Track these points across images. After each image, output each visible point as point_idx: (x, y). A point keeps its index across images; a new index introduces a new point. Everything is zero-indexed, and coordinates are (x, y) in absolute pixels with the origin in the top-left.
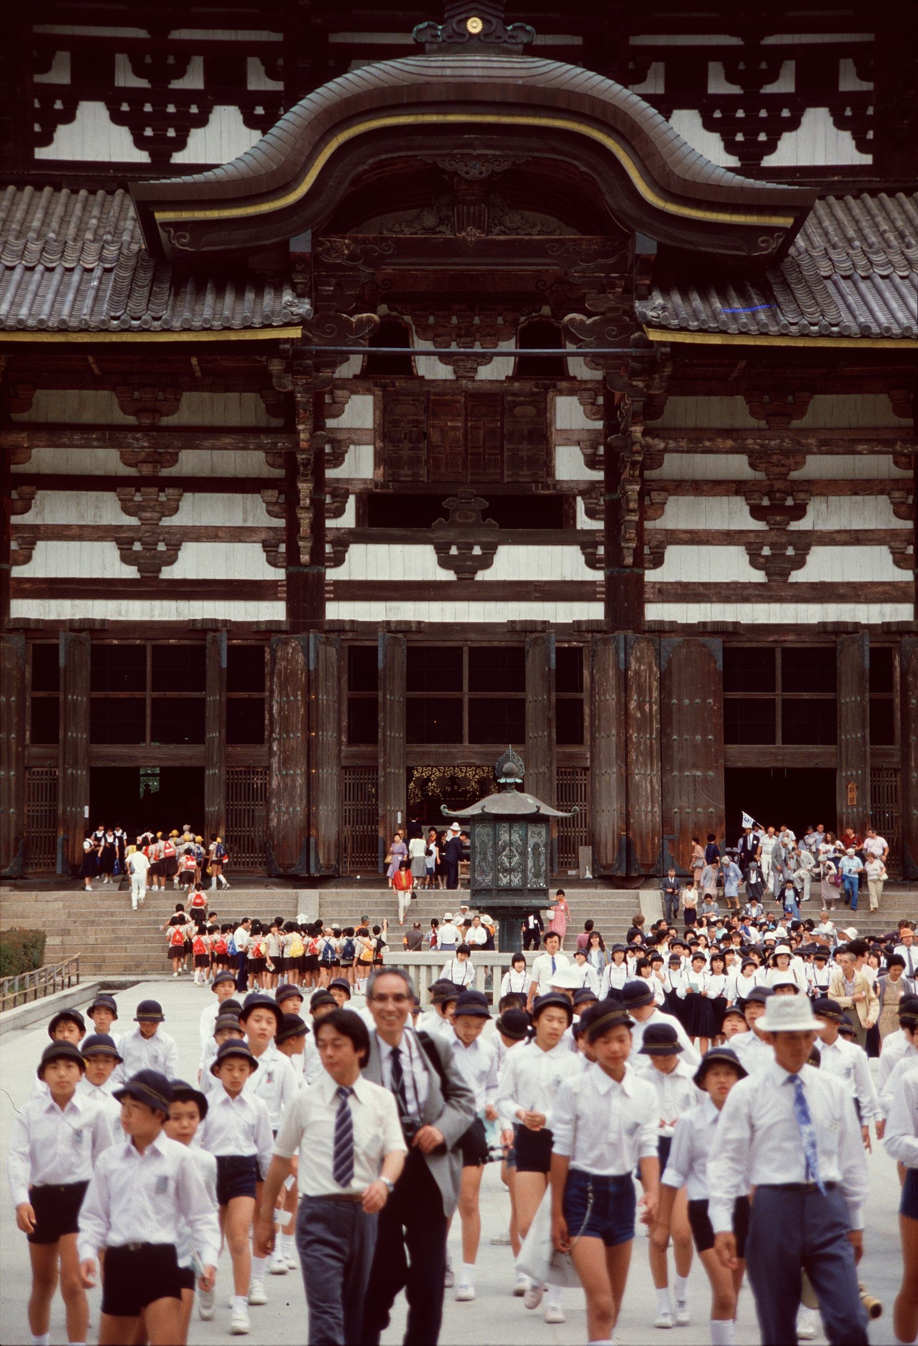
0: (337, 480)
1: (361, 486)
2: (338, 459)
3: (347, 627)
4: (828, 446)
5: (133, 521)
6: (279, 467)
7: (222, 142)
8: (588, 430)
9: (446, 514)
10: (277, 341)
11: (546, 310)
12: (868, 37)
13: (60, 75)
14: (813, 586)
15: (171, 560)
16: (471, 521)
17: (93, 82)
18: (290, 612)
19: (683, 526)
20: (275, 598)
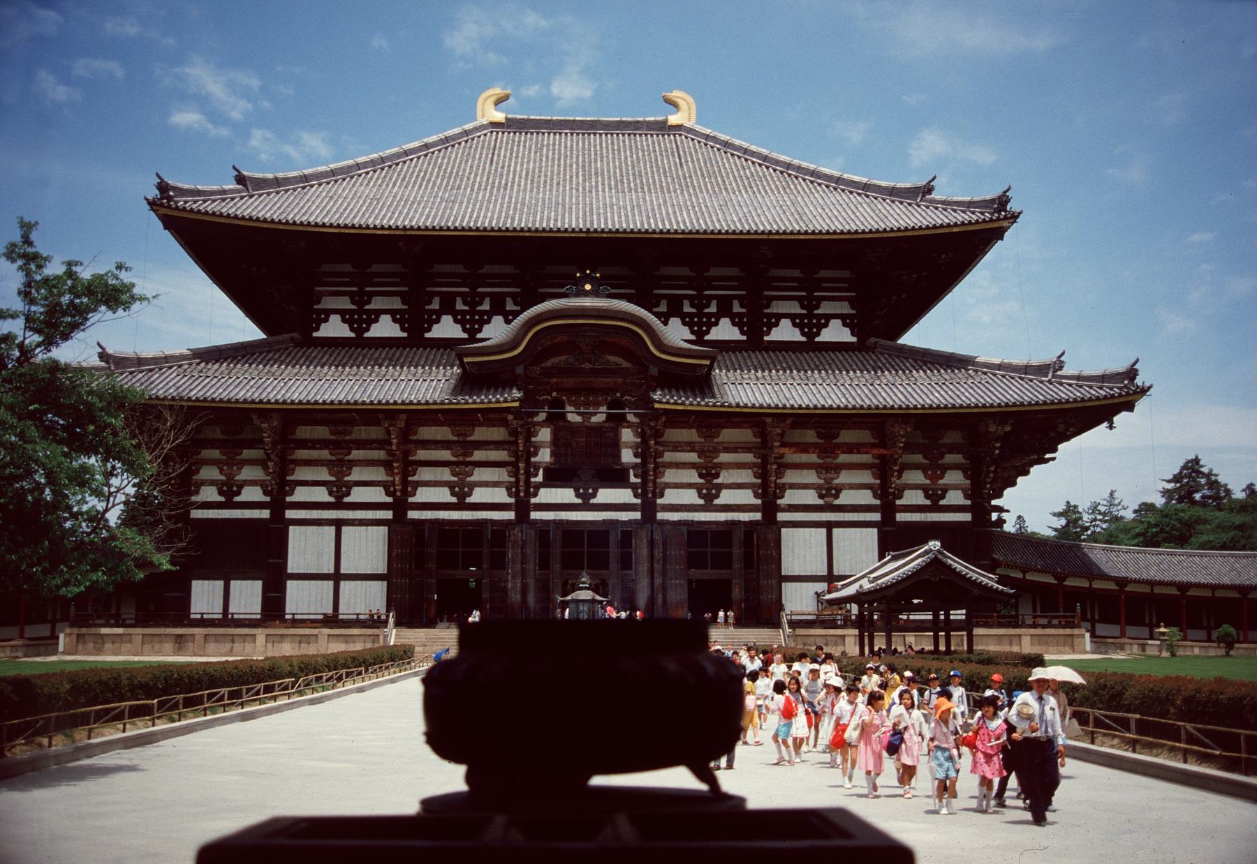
2: (536, 454)
4: (728, 450)
7: (496, 331)
12: (405, 289)
13: (435, 305)
14: (723, 505)
15: (470, 495)
17: (448, 307)
19: (672, 481)
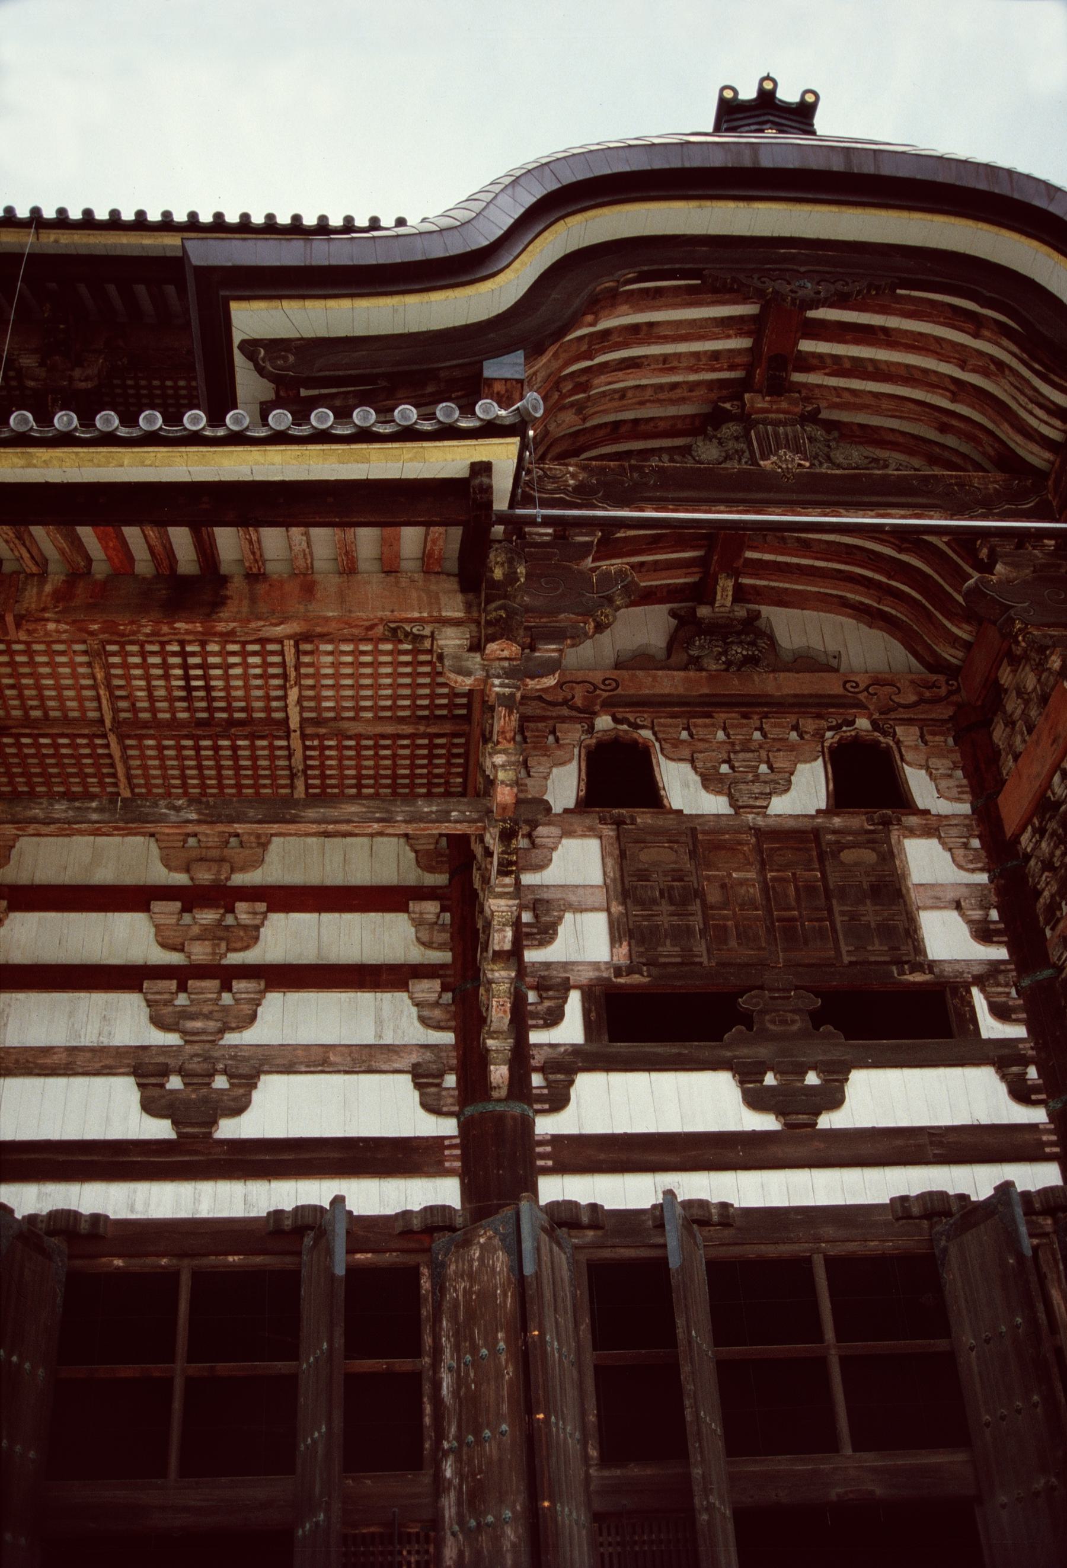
0: (548, 965)
1: (592, 974)
2: (546, 933)
3: (585, 1219)
5: (172, 1039)
6: (440, 947)
8: (967, 885)
9: (747, 1019)
11: (863, 723)
16: (795, 1027)
18: (467, 1192)
20: (440, 1171)
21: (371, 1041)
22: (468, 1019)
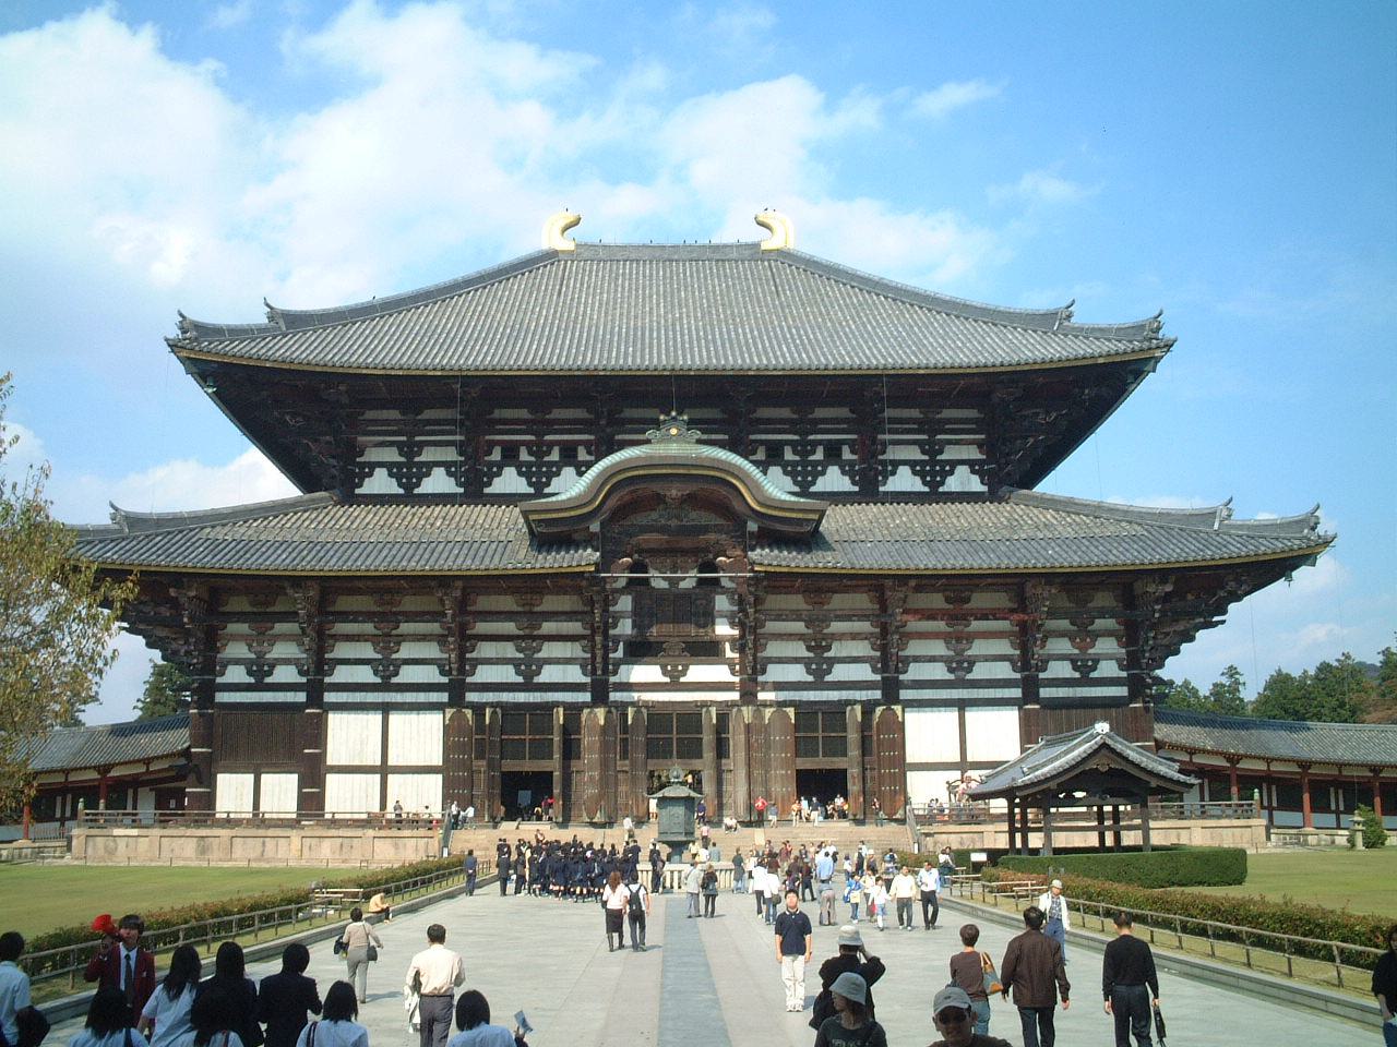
2: (615, 626)
4: (840, 618)
5: (522, 656)
10: (583, 573)
13: (496, 455)
17: (510, 455)
21: (569, 656)
22: (884, 649)
